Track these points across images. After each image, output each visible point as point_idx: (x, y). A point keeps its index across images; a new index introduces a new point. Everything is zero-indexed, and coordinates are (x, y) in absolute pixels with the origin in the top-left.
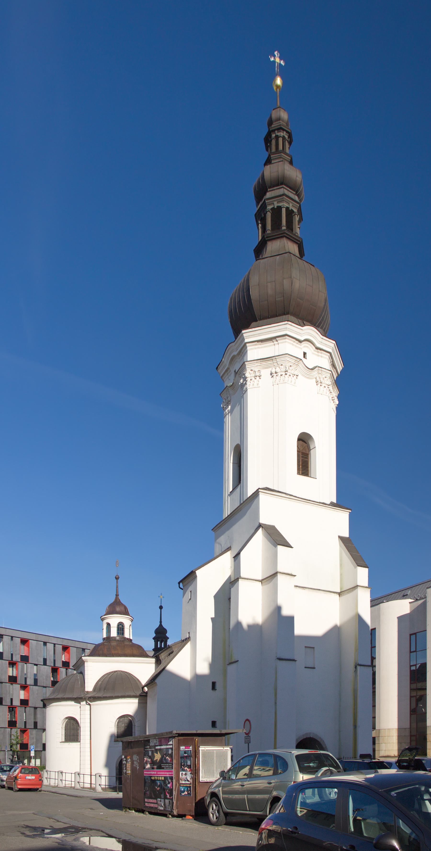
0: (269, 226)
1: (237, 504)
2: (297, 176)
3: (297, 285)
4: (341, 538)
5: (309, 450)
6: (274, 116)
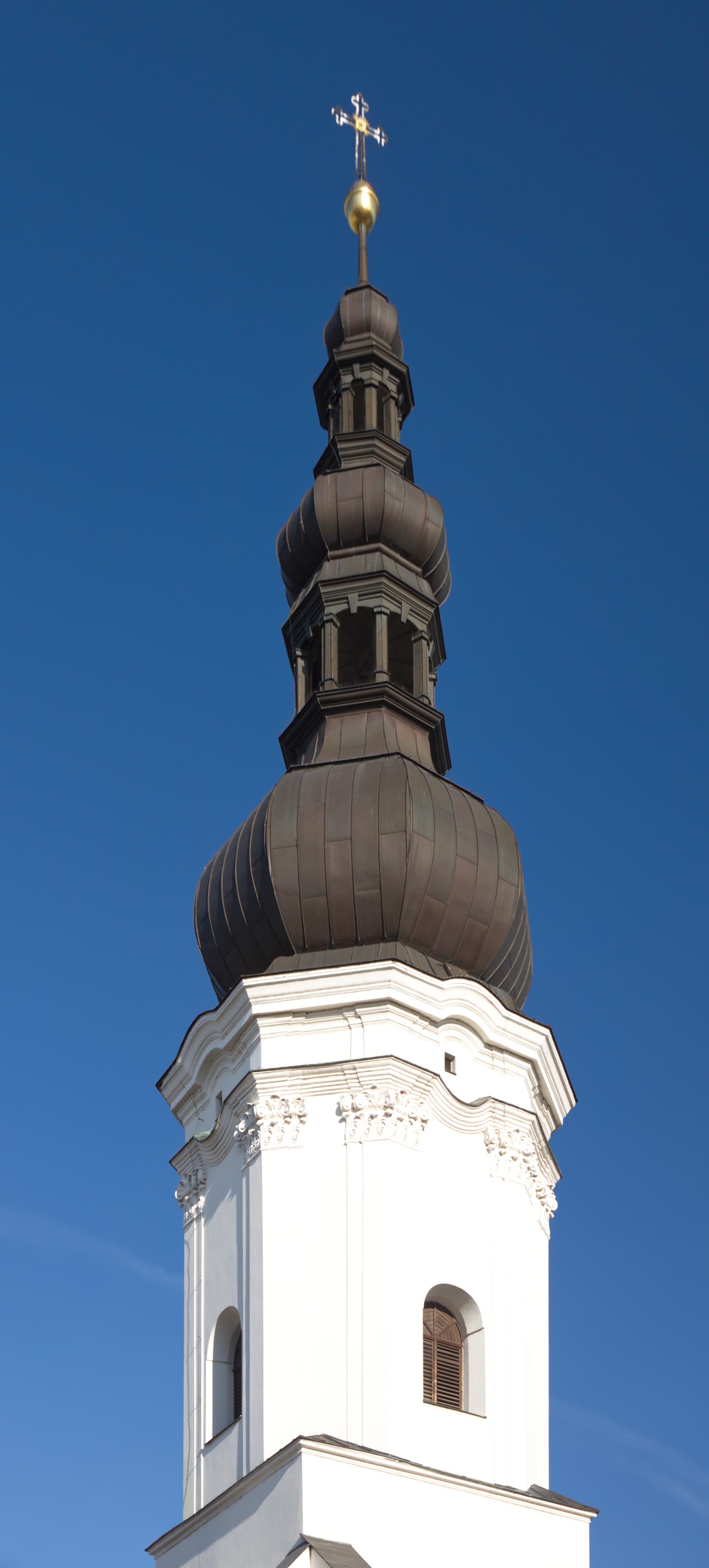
0: (331, 668)
1: (229, 1479)
3: (424, 854)
5: (463, 1335)
6: (348, 316)
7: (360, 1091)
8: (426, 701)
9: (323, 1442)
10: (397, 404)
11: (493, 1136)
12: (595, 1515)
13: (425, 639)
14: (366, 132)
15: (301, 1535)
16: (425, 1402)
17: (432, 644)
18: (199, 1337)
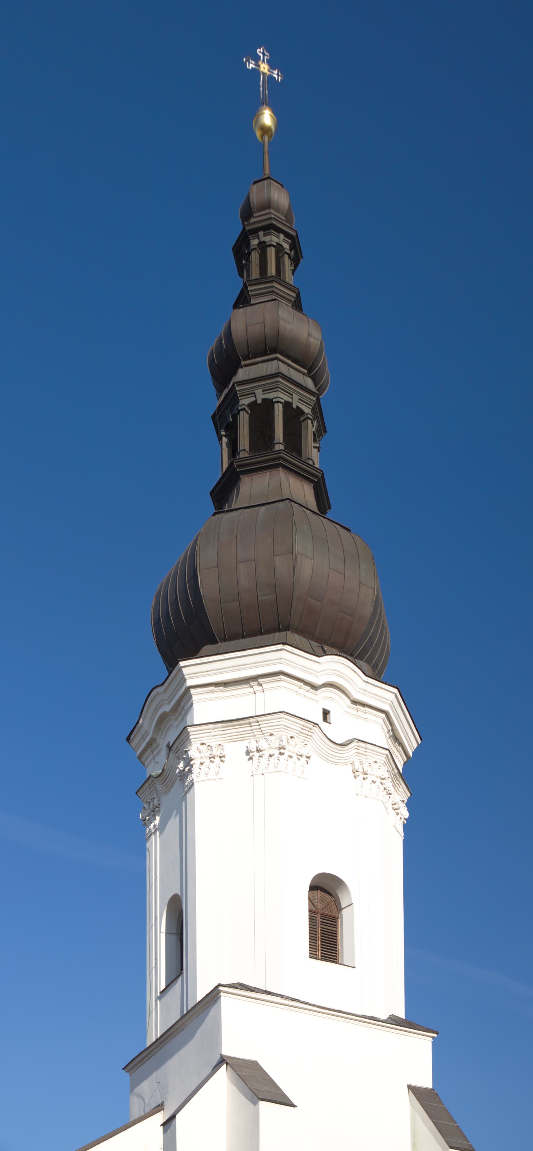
0: (244, 442)
1: (175, 1016)
2: (309, 335)
3: (306, 568)
4: (414, 1090)
5: (340, 909)
6: (255, 200)
7: (262, 738)
8: (311, 462)
9: (236, 988)
10: (289, 258)
11: (358, 766)
12: (435, 1035)
13: (310, 419)
14: (268, 73)
15: (221, 1055)
16: (310, 957)
17: (315, 424)
18: (156, 916)
